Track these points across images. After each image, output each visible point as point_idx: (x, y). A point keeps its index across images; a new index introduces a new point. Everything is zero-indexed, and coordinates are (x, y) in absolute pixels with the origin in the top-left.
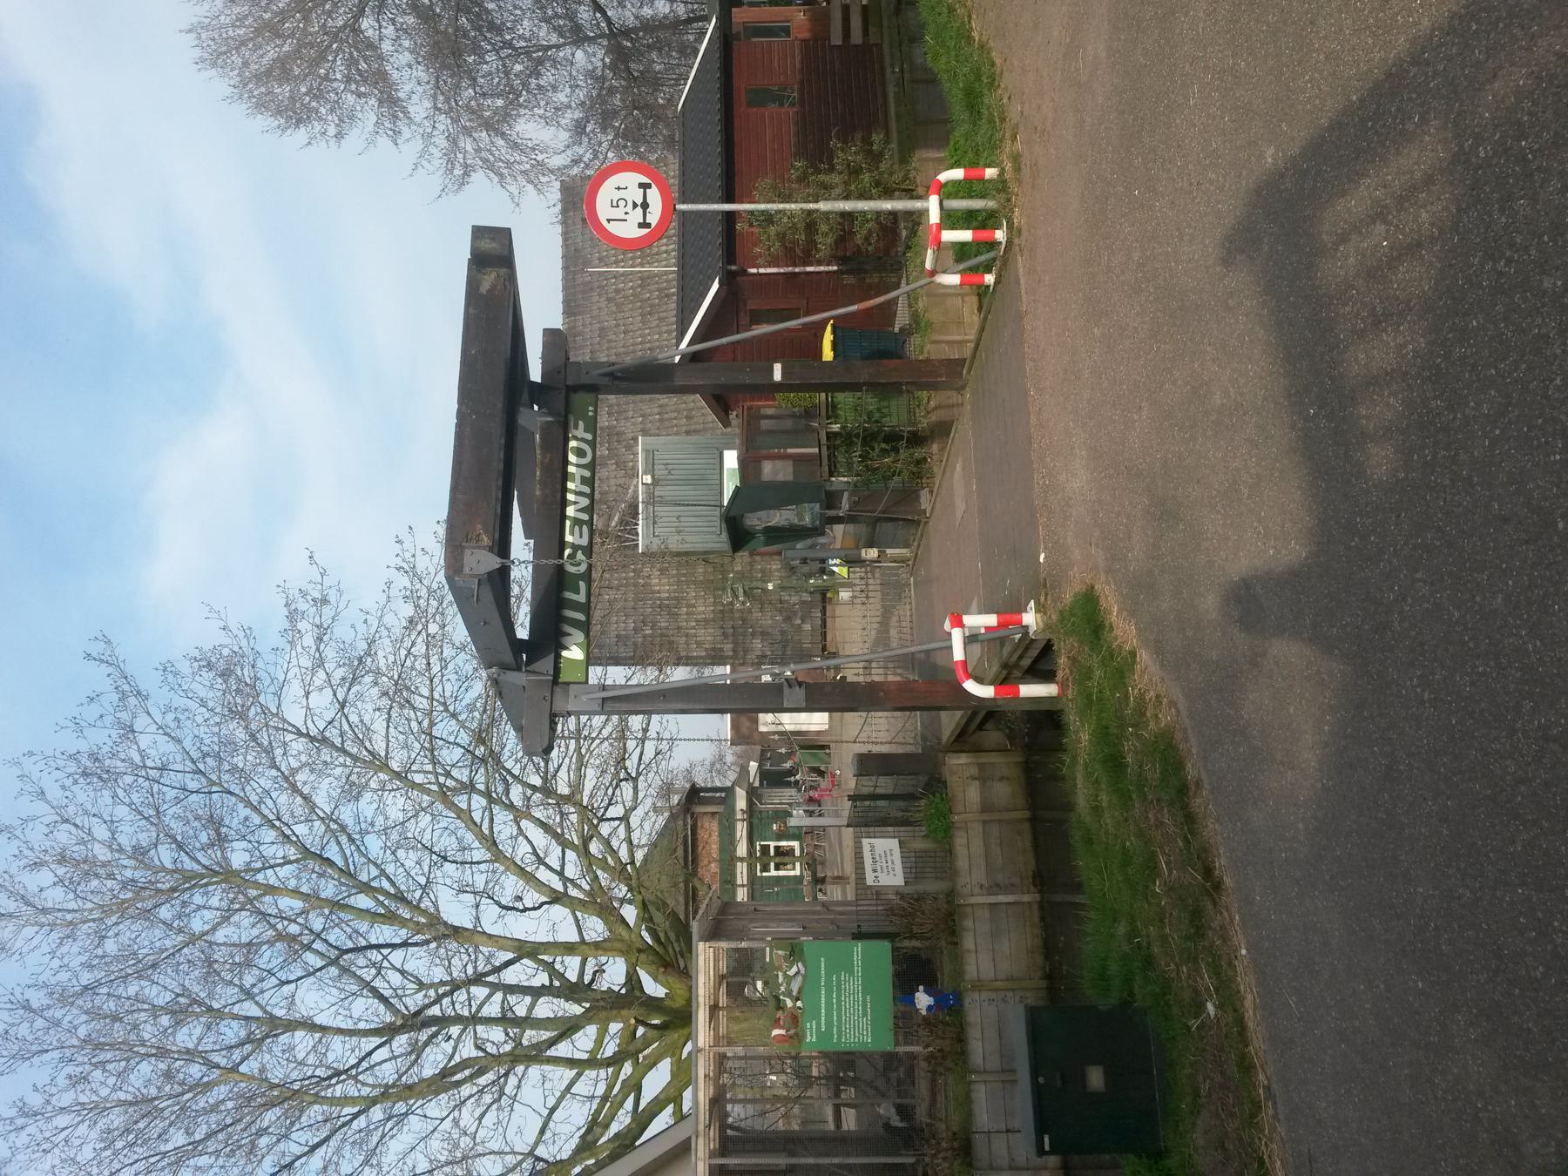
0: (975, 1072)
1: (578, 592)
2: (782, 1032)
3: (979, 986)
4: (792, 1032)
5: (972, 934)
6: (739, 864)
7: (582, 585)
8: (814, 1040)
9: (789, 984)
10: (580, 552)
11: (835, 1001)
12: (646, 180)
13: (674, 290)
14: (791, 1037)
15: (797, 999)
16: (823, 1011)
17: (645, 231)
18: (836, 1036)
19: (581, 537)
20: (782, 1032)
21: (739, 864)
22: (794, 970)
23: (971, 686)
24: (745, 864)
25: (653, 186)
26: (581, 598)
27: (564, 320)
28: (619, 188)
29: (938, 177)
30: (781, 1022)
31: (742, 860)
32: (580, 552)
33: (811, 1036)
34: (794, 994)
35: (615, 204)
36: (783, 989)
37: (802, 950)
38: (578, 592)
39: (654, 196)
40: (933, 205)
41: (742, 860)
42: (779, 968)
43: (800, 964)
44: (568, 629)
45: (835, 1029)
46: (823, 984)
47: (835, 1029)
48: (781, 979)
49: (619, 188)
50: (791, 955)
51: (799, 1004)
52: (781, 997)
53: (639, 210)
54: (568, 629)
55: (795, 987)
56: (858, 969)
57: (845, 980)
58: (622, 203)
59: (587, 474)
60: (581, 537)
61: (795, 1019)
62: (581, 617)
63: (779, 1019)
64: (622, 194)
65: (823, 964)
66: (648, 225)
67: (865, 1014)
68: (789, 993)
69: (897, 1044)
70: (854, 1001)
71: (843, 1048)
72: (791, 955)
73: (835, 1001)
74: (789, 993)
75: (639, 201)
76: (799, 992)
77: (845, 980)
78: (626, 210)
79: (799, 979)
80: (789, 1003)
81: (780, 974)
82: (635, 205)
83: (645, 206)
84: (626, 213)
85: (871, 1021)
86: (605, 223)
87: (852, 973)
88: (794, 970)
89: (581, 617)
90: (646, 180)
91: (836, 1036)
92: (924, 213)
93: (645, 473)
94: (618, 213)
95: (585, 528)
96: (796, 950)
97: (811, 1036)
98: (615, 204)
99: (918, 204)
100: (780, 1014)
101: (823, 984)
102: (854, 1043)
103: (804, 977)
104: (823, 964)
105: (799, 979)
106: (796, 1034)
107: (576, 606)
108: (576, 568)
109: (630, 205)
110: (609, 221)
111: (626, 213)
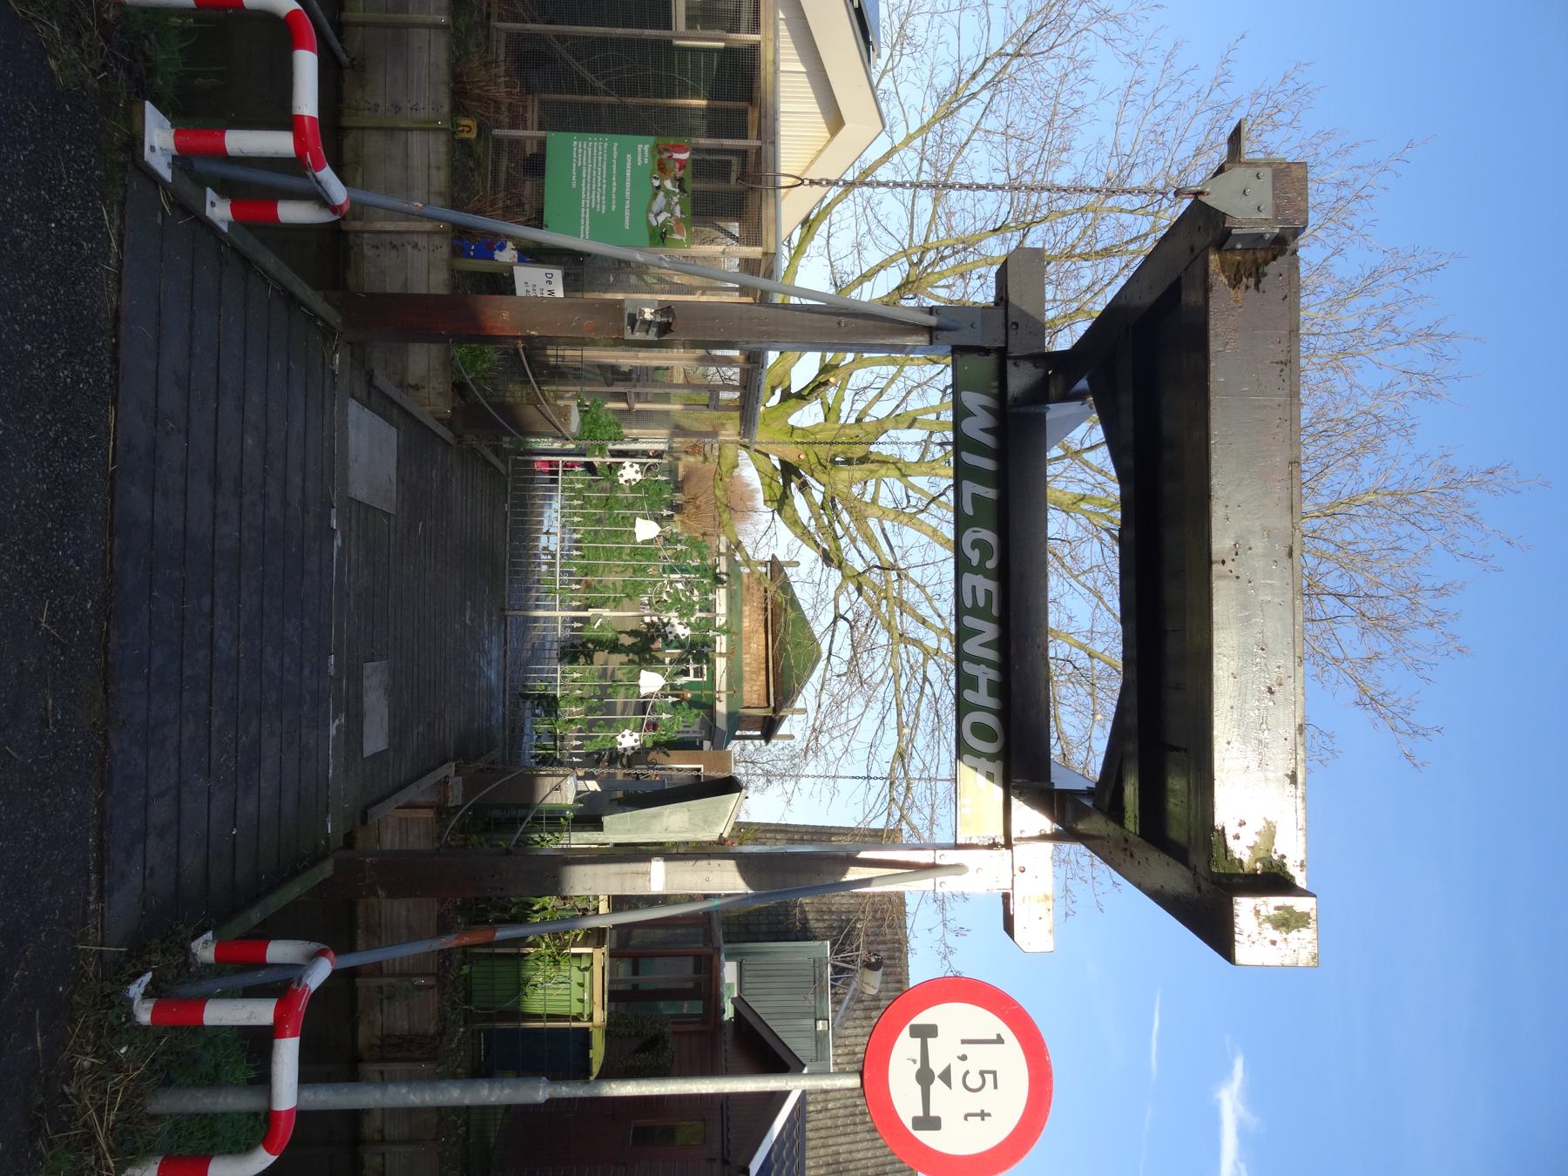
0: (437, 26)
1: (975, 497)
2: (676, 156)
3: (427, 128)
4: (666, 155)
5: (432, 189)
6: (724, 651)
7: (969, 509)
8: (640, 146)
9: (669, 204)
10: (975, 562)
11: (614, 184)
12: (925, 1137)
13: (811, 1144)
14: (667, 150)
15: (658, 188)
17: (922, 1018)
18: (615, 148)
19: (974, 588)
20: (676, 156)
21: (724, 651)
22: (661, 218)
24: (718, 651)
25: (908, 1124)
26: (969, 487)
28: (983, 1115)
30: (677, 165)
31: (721, 654)
32: (975, 562)
33: (643, 151)
34: (661, 194)
35: (989, 1078)
36: (676, 199)
38: (975, 497)
40: (286, 1092)
41: (721, 654)
42: (678, 221)
43: (655, 223)
44: (988, 440)
45: (615, 157)
46: (628, 202)
47: (615, 157)
49: (983, 1115)
50: (665, 233)
51: (657, 183)
52: (677, 191)
53: (937, 1067)
54: (988, 440)
55: (661, 200)
57: (601, 204)
58: (974, 1082)
59: (968, 695)
60: (974, 588)
61: (662, 168)
62: (969, 458)
63: (680, 169)
64: (976, 1103)
67: (579, 170)
68: (668, 194)
69: (542, 143)
70: (591, 183)
71: (607, 137)
72: (665, 233)
73: (614, 184)
74: (668, 194)
75: (937, 1086)
76: (655, 196)
77: (601, 204)
78: (963, 1066)
79: (655, 208)
80: (668, 184)
82: (946, 1077)
83: (925, 1077)
84: (964, 1058)
86: (1008, 1034)
87: (593, 211)
88: (661, 218)
89: (969, 458)
91: (615, 148)
92: (307, 1077)
93: (825, 1033)
94: (981, 1057)
95: (968, 603)
97: (643, 151)
98: (989, 1078)
100: (679, 174)
101: (628, 202)
102: (593, 141)
103: (649, 210)
105: (655, 208)
106: (660, 152)
108: (978, 536)
109: (956, 1078)
110: (999, 1040)
111: (964, 1058)
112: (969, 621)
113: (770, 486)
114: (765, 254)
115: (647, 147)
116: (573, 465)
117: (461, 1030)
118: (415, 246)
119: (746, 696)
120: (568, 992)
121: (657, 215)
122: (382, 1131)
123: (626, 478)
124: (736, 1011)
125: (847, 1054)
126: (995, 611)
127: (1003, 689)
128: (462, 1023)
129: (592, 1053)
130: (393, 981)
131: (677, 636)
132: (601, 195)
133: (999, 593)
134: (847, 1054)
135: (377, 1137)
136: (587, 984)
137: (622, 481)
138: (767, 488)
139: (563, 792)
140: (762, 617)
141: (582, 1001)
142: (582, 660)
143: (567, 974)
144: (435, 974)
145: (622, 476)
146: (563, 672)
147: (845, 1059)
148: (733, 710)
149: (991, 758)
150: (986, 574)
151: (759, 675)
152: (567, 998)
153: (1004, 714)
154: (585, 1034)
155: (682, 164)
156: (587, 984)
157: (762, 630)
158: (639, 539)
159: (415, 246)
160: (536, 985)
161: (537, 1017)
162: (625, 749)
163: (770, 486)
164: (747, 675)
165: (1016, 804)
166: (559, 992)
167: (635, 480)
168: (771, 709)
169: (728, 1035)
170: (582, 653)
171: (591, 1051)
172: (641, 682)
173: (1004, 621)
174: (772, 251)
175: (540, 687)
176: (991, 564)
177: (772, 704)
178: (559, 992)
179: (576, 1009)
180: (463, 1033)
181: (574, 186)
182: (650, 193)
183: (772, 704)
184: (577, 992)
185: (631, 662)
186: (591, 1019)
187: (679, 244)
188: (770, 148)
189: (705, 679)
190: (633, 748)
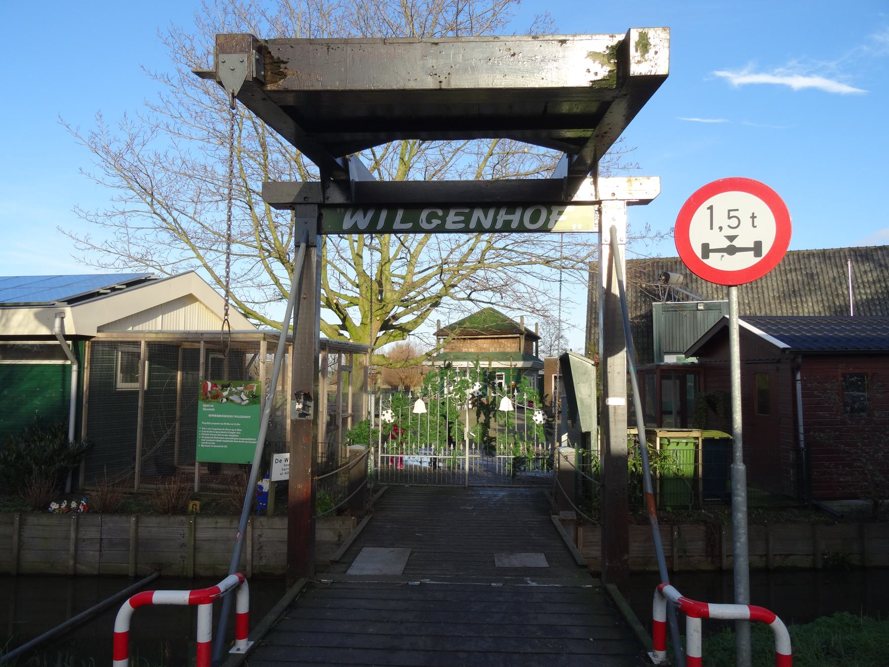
2: (209, 389)
4: (209, 395)
5: (228, 526)
7: (409, 225)
8: (204, 409)
9: (236, 393)
10: (439, 222)
11: (225, 424)
12: (765, 251)
14: (206, 394)
15: (227, 399)
16: (220, 416)
17: (698, 252)
18: (205, 423)
19: (454, 222)
20: (209, 389)
21: (488, 363)
22: (244, 398)
23: (126, 609)
24: (488, 366)
26: (397, 225)
27: (820, 250)
28: (753, 217)
29: (777, 618)
30: (214, 388)
31: (490, 364)
32: (439, 222)
33: (207, 408)
34: (231, 397)
35: (732, 214)
36: (234, 389)
37: (255, 403)
39: (745, 261)
40: (739, 611)
41: (490, 364)
42: (246, 388)
43: (247, 401)
44: (370, 214)
46: (235, 416)
48: (240, 388)
49: (753, 217)
50: (253, 396)
51: (225, 400)
52: (229, 388)
53: (726, 243)
54: (370, 214)
55: (234, 398)
56: (243, 440)
57: (237, 431)
58: (734, 222)
59: (514, 225)
60: (454, 222)
61: (216, 397)
62: (381, 225)
63: (217, 387)
64: (746, 221)
65: (246, 417)
66: (706, 254)
67: (217, 443)
68: (231, 394)
69: (202, 464)
70: (225, 437)
72: (253, 396)
74: (231, 394)
75: (737, 243)
76: (232, 401)
77: (237, 431)
78: (725, 228)
79: (239, 401)
80: (225, 393)
81: (242, 388)
82: (731, 238)
83: (731, 250)
84: (721, 228)
85: (213, 447)
87: (240, 436)
88: (244, 398)
89: (381, 225)
90: (765, 251)
91: (205, 423)
92: (731, 599)
93: (706, 305)
94: (720, 218)
95: (462, 226)
96: (255, 399)
97: (207, 408)
98: (732, 214)
99: (743, 586)
101: (235, 416)
103: (240, 404)
104: (246, 417)
105: (239, 401)
106: (207, 398)
107: (390, 221)
108: (424, 220)
109: (732, 232)
110: (711, 208)
111: (721, 228)
112: (472, 225)
113: (395, 337)
114: (264, 339)
115: (204, 405)
116: (383, 448)
117: (703, 511)
118: (260, 536)
119: (513, 350)
120: (682, 451)
121: (242, 400)
122: (761, 556)
123: (390, 419)
124: (693, 356)
125: (717, 292)
126: (467, 211)
127: (511, 206)
128: (699, 511)
129: (717, 438)
130: (675, 549)
131: (480, 390)
132: (231, 431)
133: (456, 208)
134: (717, 292)
135: (764, 559)
136: (677, 440)
137: (392, 421)
138: (396, 339)
139: (568, 454)
140: (469, 341)
141: (687, 443)
142: (493, 443)
143: (672, 451)
144: (672, 527)
145: (389, 421)
146: (500, 454)
147: (720, 293)
148: (521, 357)
149: (550, 213)
150: (446, 215)
151: (501, 343)
152: (685, 451)
153: (525, 205)
154: (706, 441)
155: (214, 385)
156: (677, 440)
157: (476, 341)
158: (425, 411)
159: (260, 536)
160: (678, 469)
161: (696, 468)
162: (544, 419)
163: (395, 337)
164: (502, 350)
165: (575, 199)
166: (682, 456)
167: (392, 414)
168: (521, 336)
169: (706, 360)
170: (489, 443)
171: (716, 438)
172: (506, 410)
173: (473, 206)
174: (263, 335)
175: (509, 467)
176: (440, 213)
177: (518, 335)
178: (682, 456)
179: (691, 446)
180: (704, 510)
181: (226, 446)
182: (230, 404)
183: (518, 335)
184: (682, 446)
185: (494, 416)
186: (697, 438)
187: (259, 388)
188: (204, 336)
189: (504, 373)
190: (543, 415)
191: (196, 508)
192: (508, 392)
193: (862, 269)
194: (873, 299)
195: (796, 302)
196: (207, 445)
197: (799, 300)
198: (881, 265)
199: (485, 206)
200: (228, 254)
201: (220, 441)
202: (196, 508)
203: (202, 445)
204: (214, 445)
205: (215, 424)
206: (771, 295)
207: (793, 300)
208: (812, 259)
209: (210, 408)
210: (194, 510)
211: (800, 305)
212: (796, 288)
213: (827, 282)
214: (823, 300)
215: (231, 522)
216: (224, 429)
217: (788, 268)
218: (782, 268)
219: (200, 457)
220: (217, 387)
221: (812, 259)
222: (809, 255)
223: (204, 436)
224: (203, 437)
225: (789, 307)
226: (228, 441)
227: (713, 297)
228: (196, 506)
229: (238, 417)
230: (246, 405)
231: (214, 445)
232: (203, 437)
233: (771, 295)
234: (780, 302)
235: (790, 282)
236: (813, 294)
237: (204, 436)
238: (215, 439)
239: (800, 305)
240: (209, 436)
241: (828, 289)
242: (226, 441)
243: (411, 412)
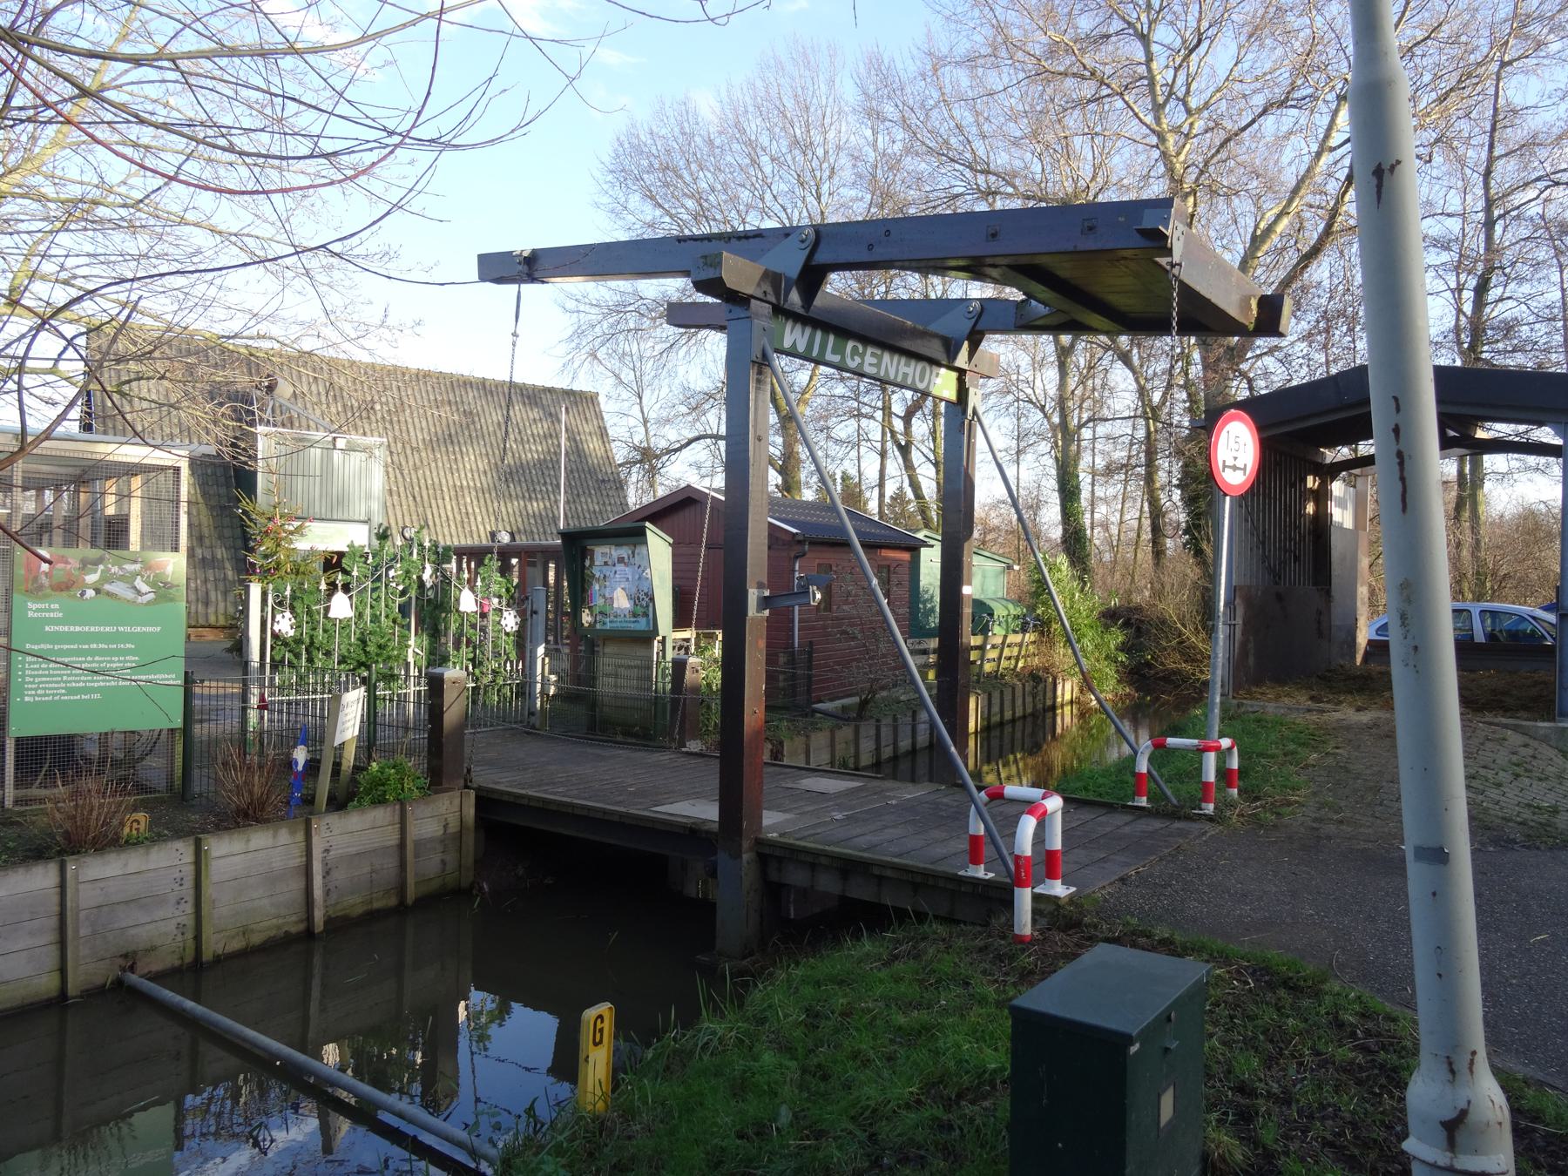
5: (270, 845)
8: (30, 614)
9: (122, 578)
15: (98, 591)
16: (78, 629)
22: (144, 588)
33: (37, 610)
34: (107, 587)
36: (115, 569)
43: (152, 596)
46: (121, 629)
51: (90, 593)
52: (101, 567)
55: (117, 588)
63: (67, 563)
67: (71, 691)
68: (108, 578)
74: (108, 578)
79: (130, 595)
80: (92, 578)
88: (144, 588)
97: (37, 610)
101: (121, 629)
105: (130, 595)
121: (139, 593)
182: (108, 601)
191: (137, 829)
192: (469, 581)
193: (531, 416)
194: (545, 460)
195: (454, 453)
196: (45, 695)
197: (457, 449)
198: (550, 414)
199: (866, 340)
200: (1135, 417)
201: (81, 684)
202: (137, 829)
203: (27, 699)
204: (64, 695)
205: (66, 647)
206: (420, 437)
207: (451, 449)
208: (469, 390)
209: (50, 610)
210: (134, 832)
211: (459, 457)
212: (453, 432)
213: (491, 429)
214: (487, 454)
215: (274, 837)
216: (89, 659)
217: (439, 398)
218: (432, 398)
219: (19, 727)
220: (67, 563)
221: (469, 390)
222: (465, 383)
223: (31, 676)
224: (28, 679)
225: (445, 458)
226: (102, 684)
227: (300, 426)
228: (139, 823)
229: (128, 629)
230: (149, 603)
231: (64, 695)
232: (28, 679)
233: (420, 437)
234: (433, 450)
235: (444, 420)
236: (475, 443)
237: (31, 676)
238: (66, 682)
239: (459, 457)
240: (49, 676)
241: (493, 438)
242: (96, 685)
243: (326, 616)
